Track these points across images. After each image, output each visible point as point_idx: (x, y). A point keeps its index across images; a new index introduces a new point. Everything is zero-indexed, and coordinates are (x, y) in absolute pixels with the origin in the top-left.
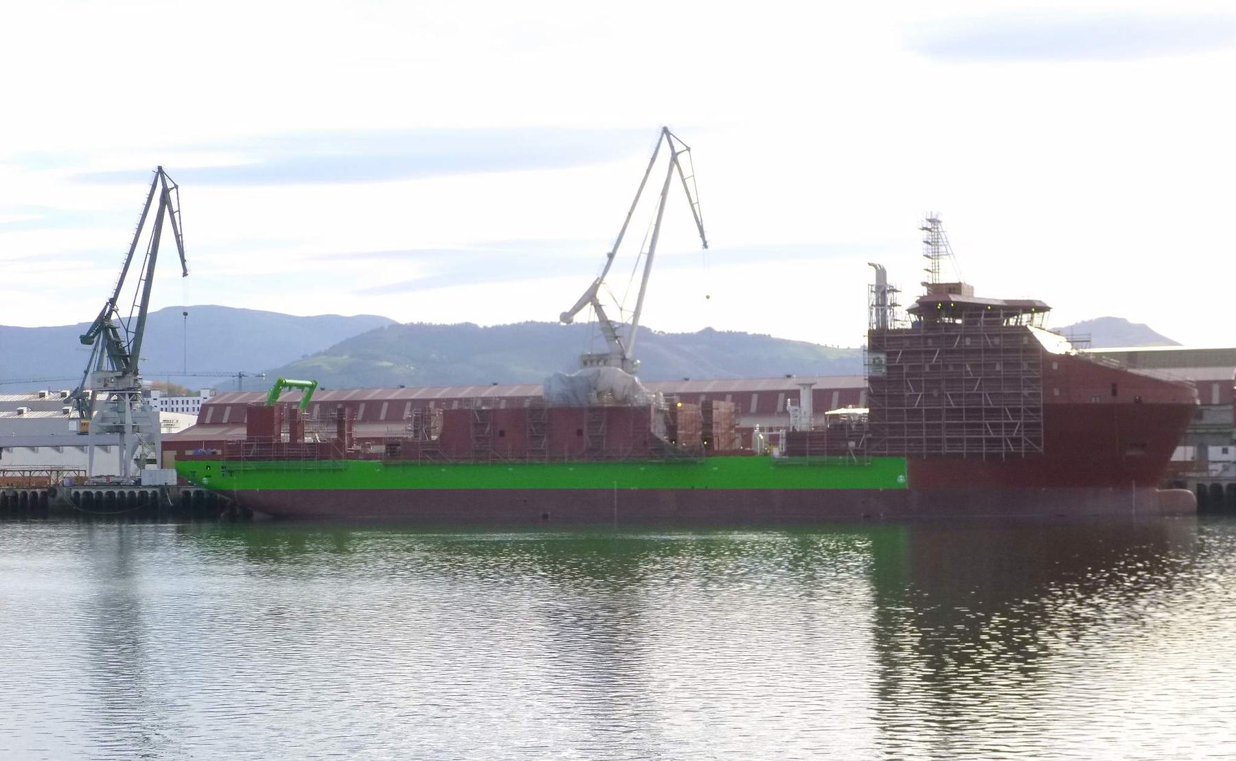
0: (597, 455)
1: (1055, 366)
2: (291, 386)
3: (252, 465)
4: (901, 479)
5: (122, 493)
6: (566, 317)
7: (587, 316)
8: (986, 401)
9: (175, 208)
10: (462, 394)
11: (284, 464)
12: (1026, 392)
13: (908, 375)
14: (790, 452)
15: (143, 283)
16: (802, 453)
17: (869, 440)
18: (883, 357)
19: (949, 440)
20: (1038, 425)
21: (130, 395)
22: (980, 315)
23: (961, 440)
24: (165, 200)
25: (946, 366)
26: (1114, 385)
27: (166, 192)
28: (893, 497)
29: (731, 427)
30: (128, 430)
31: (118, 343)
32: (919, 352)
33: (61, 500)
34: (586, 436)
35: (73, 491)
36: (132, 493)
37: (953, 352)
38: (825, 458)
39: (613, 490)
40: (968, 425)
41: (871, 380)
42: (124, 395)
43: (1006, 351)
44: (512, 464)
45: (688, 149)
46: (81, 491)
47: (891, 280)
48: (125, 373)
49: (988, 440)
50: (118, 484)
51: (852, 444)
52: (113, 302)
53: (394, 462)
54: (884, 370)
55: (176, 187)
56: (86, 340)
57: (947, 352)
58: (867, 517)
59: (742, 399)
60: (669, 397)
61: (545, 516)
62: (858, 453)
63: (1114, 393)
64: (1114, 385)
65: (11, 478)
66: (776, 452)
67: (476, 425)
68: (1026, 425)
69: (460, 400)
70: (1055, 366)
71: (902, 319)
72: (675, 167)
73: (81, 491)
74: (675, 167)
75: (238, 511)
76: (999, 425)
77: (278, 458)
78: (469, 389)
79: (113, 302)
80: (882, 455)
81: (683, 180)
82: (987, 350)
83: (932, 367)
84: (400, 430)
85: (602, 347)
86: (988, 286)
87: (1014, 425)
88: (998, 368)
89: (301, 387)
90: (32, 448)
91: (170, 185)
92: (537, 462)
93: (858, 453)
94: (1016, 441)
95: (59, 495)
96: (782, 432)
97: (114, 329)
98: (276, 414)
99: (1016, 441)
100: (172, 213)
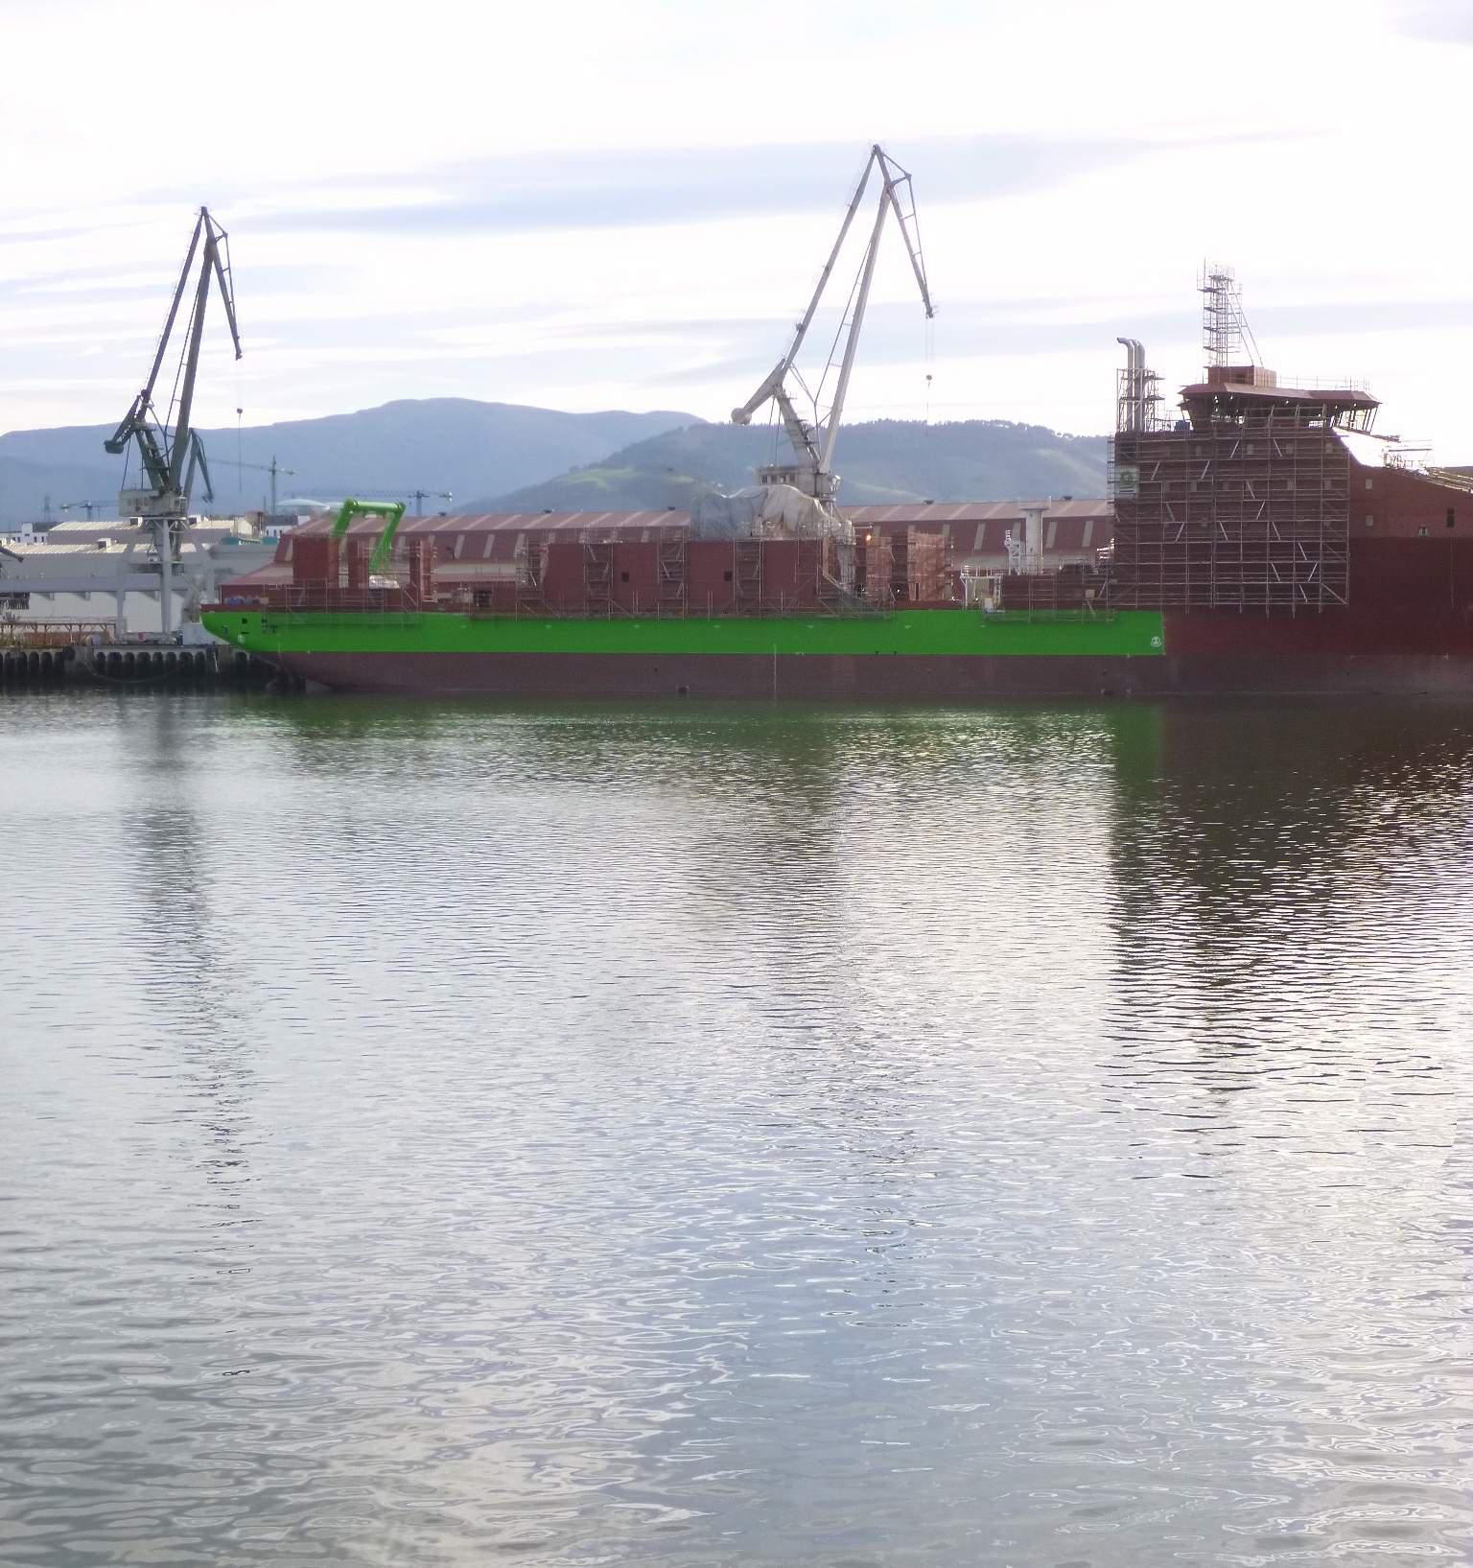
0: (755, 609)
1: (1369, 485)
2: (366, 510)
3: (300, 618)
4: (1156, 642)
5: (159, 656)
6: (741, 416)
7: (767, 414)
8: (1272, 532)
9: (224, 265)
10: (627, 522)
11: (342, 617)
12: (1328, 521)
13: (1169, 497)
14: (1007, 604)
15: (184, 369)
16: (1023, 606)
17: (1111, 587)
18: (1134, 471)
19: (1220, 588)
20: (1342, 567)
21: (170, 522)
22: (1267, 413)
23: (1236, 588)
24: (211, 254)
25: (1220, 485)
26: (1451, 512)
27: (211, 242)
28: (1144, 665)
29: (939, 569)
30: (168, 570)
31: (155, 451)
32: (1183, 465)
33: (80, 664)
34: (736, 582)
35: (96, 652)
36: (172, 656)
37: (1230, 464)
38: (1053, 613)
39: (769, 658)
40: (1247, 568)
41: (1118, 504)
42: (161, 522)
43: (1300, 463)
44: (638, 619)
45: (908, 177)
46: (106, 653)
47: (1150, 364)
48: (162, 493)
49: (1274, 588)
50: (156, 643)
51: (1090, 593)
52: (146, 394)
53: (482, 615)
54: (1136, 490)
55: (225, 235)
56: (113, 447)
57: (1222, 464)
58: (1108, 694)
59: (963, 531)
60: (861, 529)
61: (683, 691)
62: (1098, 605)
63: (1451, 523)
64: (1451, 512)
65: (55, 634)
66: (989, 604)
67: (590, 565)
68: (1327, 567)
69: (559, 531)
70: (1369, 485)
71: (1169, 412)
72: (891, 208)
73: (106, 653)
74: (891, 208)
75: (291, 680)
76: (1289, 567)
77: (334, 609)
78: (963, 508)
79: (146, 394)
80: (1131, 608)
81: (901, 222)
82: (1276, 462)
83: (1200, 485)
84: (508, 571)
85: (788, 456)
86: (1294, 368)
87: (1309, 567)
88: (1291, 486)
89: (382, 511)
90: (82, 594)
91: (217, 233)
92: (670, 615)
93: (1098, 605)
94: (1312, 590)
95: (77, 657)
96: (998, 577)
97: (148, 433)
98: (331, 549)
99: (1312, 590)
100: (220, 272)
